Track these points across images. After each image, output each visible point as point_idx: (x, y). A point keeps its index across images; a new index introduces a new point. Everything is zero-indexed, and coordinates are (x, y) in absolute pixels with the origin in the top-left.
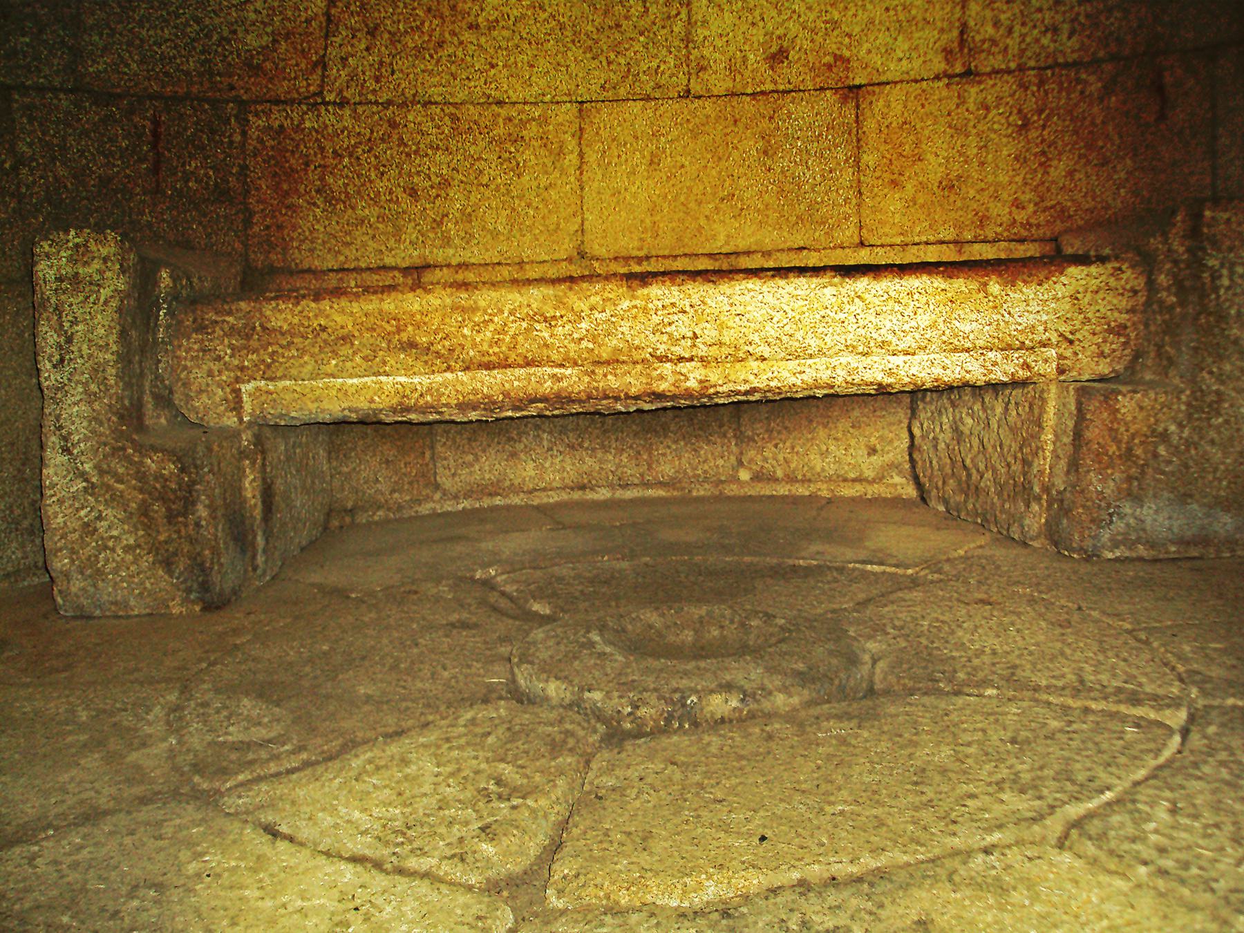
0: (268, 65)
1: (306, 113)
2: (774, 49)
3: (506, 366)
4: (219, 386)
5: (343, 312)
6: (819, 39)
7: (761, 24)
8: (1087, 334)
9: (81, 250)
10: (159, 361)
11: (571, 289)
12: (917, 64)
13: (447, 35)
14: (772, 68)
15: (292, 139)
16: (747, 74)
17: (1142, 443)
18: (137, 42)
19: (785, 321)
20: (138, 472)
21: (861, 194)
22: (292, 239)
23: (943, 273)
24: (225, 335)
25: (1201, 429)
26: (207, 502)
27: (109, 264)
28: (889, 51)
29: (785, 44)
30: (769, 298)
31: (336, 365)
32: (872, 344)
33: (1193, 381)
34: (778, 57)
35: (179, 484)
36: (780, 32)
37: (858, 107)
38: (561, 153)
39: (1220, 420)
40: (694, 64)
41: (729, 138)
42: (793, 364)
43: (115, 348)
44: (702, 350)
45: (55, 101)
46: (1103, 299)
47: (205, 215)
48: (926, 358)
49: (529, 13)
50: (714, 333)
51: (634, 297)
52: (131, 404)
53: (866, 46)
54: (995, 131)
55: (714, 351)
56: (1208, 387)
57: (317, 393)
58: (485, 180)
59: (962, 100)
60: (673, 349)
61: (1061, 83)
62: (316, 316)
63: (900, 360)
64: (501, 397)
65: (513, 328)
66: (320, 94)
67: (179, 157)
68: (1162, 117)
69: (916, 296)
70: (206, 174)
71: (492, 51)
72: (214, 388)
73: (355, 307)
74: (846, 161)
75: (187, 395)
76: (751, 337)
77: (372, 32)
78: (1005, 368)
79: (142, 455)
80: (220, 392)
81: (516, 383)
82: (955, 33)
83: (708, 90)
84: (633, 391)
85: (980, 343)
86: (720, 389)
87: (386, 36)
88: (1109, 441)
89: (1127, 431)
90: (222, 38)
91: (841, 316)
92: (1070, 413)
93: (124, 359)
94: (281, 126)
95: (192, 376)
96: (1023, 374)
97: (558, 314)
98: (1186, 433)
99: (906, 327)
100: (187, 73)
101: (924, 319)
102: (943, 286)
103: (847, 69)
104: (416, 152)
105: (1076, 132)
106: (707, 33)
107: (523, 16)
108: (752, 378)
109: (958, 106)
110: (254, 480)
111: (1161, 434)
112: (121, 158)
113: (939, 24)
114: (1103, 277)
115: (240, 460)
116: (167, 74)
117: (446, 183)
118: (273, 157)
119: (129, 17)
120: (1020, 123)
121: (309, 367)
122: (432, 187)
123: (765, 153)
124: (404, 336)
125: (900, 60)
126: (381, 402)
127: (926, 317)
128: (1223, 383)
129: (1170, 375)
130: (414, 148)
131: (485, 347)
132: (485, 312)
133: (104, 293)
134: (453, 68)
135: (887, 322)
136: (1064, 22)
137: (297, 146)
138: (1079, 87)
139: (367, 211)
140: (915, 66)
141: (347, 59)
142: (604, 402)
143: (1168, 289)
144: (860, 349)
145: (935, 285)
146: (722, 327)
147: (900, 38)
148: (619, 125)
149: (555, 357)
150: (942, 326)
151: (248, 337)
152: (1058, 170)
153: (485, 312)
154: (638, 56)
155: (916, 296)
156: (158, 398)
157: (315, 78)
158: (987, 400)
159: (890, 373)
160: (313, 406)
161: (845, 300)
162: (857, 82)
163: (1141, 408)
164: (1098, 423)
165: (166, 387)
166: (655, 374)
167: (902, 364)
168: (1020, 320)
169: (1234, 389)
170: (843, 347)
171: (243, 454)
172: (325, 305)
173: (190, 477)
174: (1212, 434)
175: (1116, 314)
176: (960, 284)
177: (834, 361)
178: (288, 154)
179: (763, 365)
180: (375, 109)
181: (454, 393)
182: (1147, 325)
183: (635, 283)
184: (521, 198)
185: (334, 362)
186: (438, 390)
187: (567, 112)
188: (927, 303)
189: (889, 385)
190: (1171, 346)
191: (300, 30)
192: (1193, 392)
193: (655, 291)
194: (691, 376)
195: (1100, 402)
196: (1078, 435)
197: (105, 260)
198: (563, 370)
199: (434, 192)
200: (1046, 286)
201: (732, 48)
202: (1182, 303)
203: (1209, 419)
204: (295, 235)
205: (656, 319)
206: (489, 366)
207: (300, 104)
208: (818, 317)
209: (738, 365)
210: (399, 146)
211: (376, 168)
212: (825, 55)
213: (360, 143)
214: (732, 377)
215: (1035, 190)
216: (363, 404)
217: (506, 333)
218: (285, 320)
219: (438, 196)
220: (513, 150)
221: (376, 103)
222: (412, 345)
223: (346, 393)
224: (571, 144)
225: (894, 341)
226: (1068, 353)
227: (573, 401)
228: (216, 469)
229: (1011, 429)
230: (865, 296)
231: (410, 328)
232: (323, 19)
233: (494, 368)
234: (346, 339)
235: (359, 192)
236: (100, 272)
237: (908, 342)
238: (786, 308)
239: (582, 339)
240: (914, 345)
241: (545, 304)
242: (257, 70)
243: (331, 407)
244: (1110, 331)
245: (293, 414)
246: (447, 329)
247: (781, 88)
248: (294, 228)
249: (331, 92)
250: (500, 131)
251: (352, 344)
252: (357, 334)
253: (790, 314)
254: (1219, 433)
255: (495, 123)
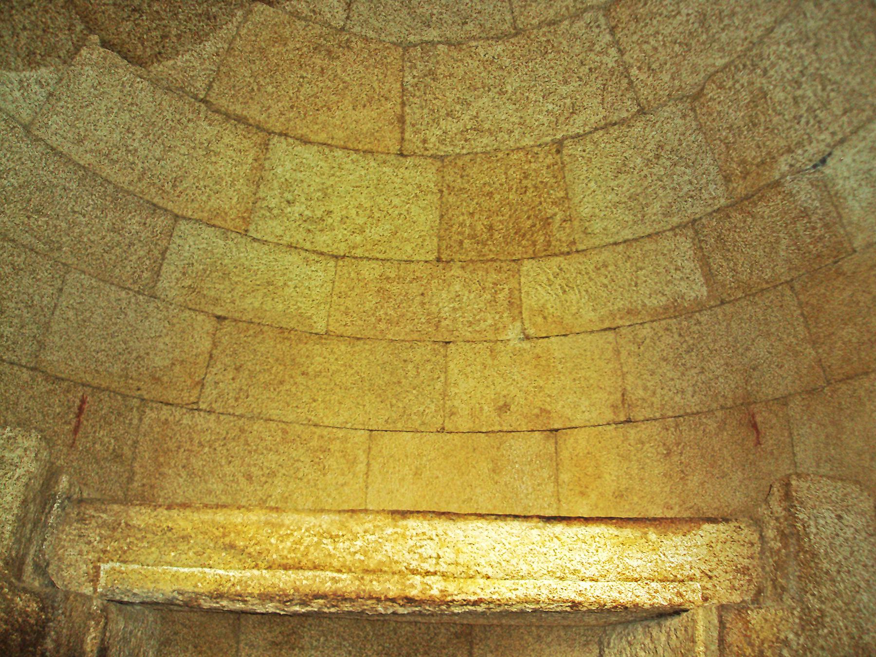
0: (165, 379)
1: (185, 414)
2: (501, 403)
3: (298, 569)
4: (85, 562)
5: (186, 518)
6: (530, 398)
7: (493, 387)
8: (721, 572)
9: (11, 441)
10: (45, 540)
11: (351, 517)
12: (594, 415)
13: (287, 377)
14: (499, 416)
15: (173, 430)
16: (483, 418)
17: (770, 647)
18: (83, 348)
19: (504, 551)
20: (8, 606)
21: (559, 501)
22: (159, 496)
23: (615, 524)
24: (98, 526)
25: (812, 637)
26: (54, 637)
27: (28, 452)
28: (576, 406)
29: (508, 401)
30: (492, 534)
31: (175, 556)
32: (567, 571)
33: (801, 601)
34: (504, 408)
35: (37, 620)
36: (505, 392)
37: (556, 443)
38: (354, 461)
39: (826, 631)
40: (448, 410)
41: (470, 461)
42: (509, 583)
43: (16, 512)
44: (443, 568)
45: (19, 373)
46: (730, 548)
47: (102, 468)
48: (606, 584)
49: (342, 369)
50: (453, 556)
51: (396, 526)
52: (16, 556)
53: (561, 403)
54: (648, 458)
55: (452, 569)
56: (813, 606)
57: (156, 576)
58: (300, 475)
59: (626, 438)
60: (422, 565)
61: (690, 425)
62: (166, 520)
63: (587, 584)
64: (292, 591)
65: (307, 541)
66: (197, 403)
67: (93, 426)
68: (758, 443)
69: (597, 539)
70: (109, 442)
71: (315, 390)
72: (80, 563)
73: (196, 516)
74: (550, 477)
75: (59, 567)
76: (479, 561)
77: (237, 369)
78: (664, 597)
79: (15, 594)
80: (84, 567)
81: (305, 582)
82: (619, 395)
83: (457, 428)
84: (391, 595)
85: (645, 575)
86: (456, 598)
87: (247, 372)
88: (745, 645)
89: (758, 637)
90: (139, 356)
91: (544, 550)
92: (715, 626)
93: (21, 521)
94: (167, 420)
95: (66, 553)
96: (677, 600)
97: (341, 534)
98: (802, 641)
99: (591, 561)
100: (111, 374)
101: (603, 555)
102: (616, 533)
103: (549, 418)
104: (255, 451)
105: (703, 456)
106: (457, 391)
107: (338, 371)
108: (479, 591)
109: (623, 442)
110: (95, 638)
111: (783, 640)
112: (53, 418)
113: (608, 389)
114: (729, 532)
115: (88, 619)
116: (97, 371)
117: (273, 474)
118: (157, 439)
119: (81, 331)
120: (665, 452)
121: (154, 556)
122: (263, 475)
123: (494, 471)
124: (227, 540)
125: (584, 412)
126: (202, 588)
127: (605, 554)
128: (823, 602)
129: (784, 599)
130: (254, 448)
131: (285, 553)
132: (288, 528)
133: (19, 472)
134: (288, 398)
135: (577, 556)
136: (689, 386)
137: (175, 434)
138: (702, 427)
139: (215, 486)
140: (593, 416)
141: (218, 383)
142: (369, 602)
143: (775, 539)
144: (558, 574)
145: (611, 532)
146: (458, 552)
147: (583, 398)
148: (396, 447)
149: (335, 564)
150: (616, 562)
151: (114, 529)
152: (694, 481)
153: (288, 528)
154: (411, 403)
155: (597, 539)
156: (37, 566)
157: (196, 392)
158: (654, 634)
159: (580, 594)
160: (151, 586)
161: (547, 539)
162: (556, 426)
163: (766, 620)
164: (735, 630)
165: (45, 560)
166: (408, 582)
167: (589, 588)
168: (672, 560)
169: (832, 607)
170: (545, 572)
171: (90, 615)
172: (174, 513)
173: (46, 615)
174: (821, 642)
175: (741, 559)
176: (628, 532)
177: (539, 583)
178: (168, 439)
179: (488, 582)
180: (232, 418)
181: (257, 585)
182: (763, 568)
183: (398, 517)
184: (324, 490)
185: (173, 554)
186: (246, 582)
187: (361, 436)
188: (605, 544)
189: (580, 603)
190: (781, 578)
191: (191, 360)
192: (802, 609)
193: (413, 524)
194: (434, 586)
195: (735, 615)
196: (721, 640)
197: (26, 450)
198: (340, 575)
199: (263, 479)
200: (689, 537)
201: (473, 401)
202: (786, 546)
203: (817, 630)
204: (162, 494)
205: (411, 543)
206: (286, 567)
207: (182, 407)
208: (528, 549)
209: (469, 581)
210: (244, 445)
211: (227, 458)
212: (535, 408)
213: (218, 439)
214: (465, 590)
215: (679, 496)
216: (189, 588)
217: (301, 544)
218: (144, 520)
219: (266, 482)
220: (322, 457)
221: (234, 415)
222: (232, 546)
223: (177, 579)
224: (362, 457)
225: (583, 570)
226: (709, 585)
227: (346, 599)
228: (68, 614)
229: (673, 650)
230: (561, 537)
231: (232, 535)
232: (207, 356)
233: (290, 568)
234: (185, 538)
235: (212, 472)
236: (20, 457)
237: (592, 571)
238: (504, 541)
239: (356, 553)
240: (597, 574)
241: (332, 525)
242: (157, 380)
243: (165, 588)
244: (737, 571)
245: (136, 591)
246: (259, 538)
247: (505, 429)
248: (162, 488)
249: (203, 402)
250: (314, 443)
251: (189, 542)
252: (193, 535)
253: (508, 546)
254: (826, 641)
255: (311, 438)
